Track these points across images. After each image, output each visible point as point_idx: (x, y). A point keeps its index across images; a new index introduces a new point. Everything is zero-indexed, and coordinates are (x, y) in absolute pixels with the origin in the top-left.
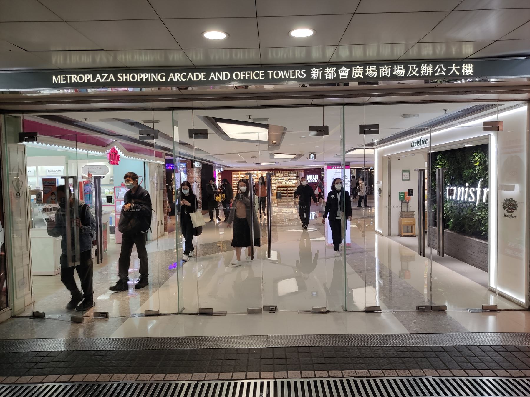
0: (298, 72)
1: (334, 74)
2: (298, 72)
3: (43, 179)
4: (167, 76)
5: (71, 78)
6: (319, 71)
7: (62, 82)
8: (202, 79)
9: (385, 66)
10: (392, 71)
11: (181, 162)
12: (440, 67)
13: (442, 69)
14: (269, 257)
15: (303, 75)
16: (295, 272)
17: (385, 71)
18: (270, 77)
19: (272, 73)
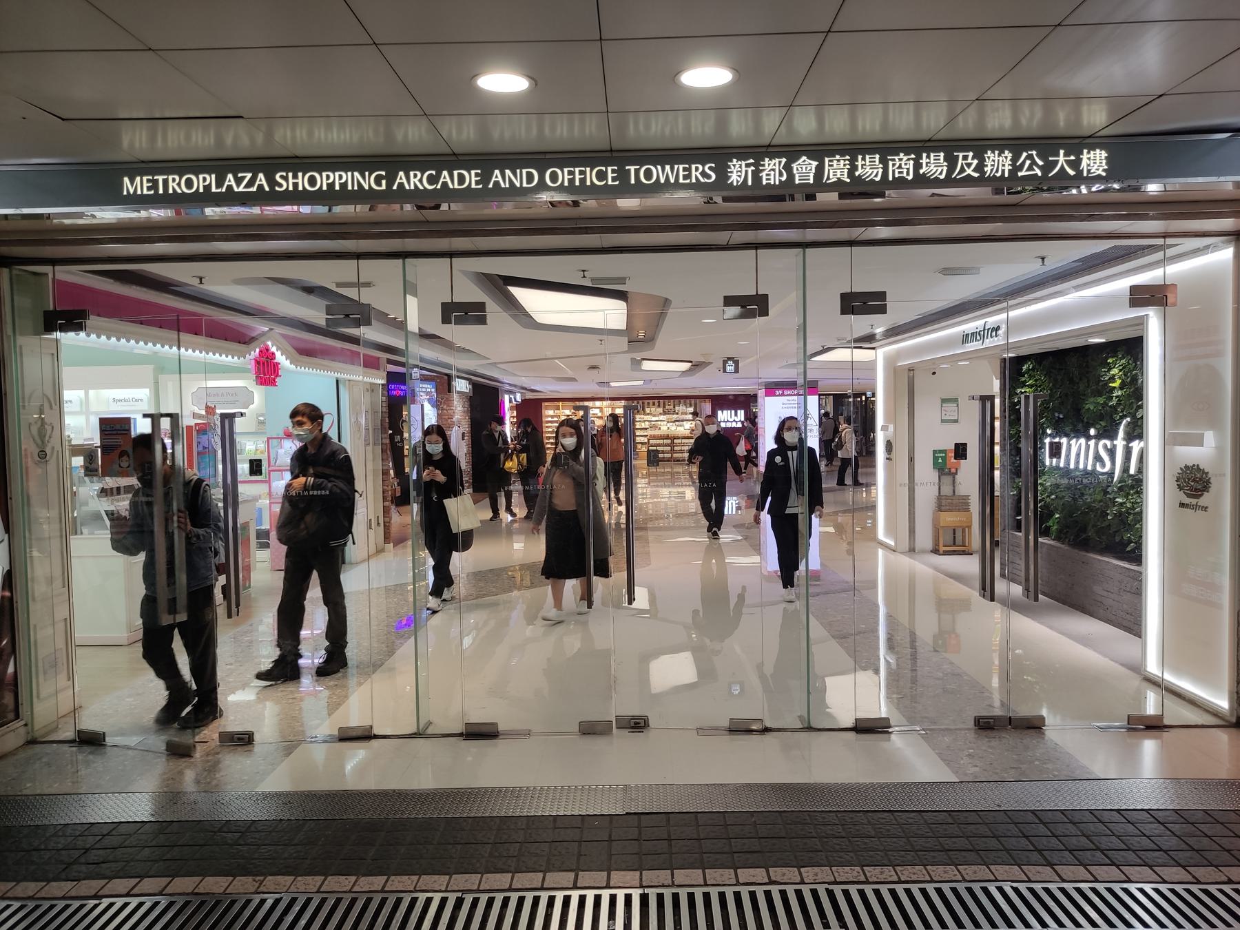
0: (697, 169)
1: (781, 174)
2: (697, 169)
4: (391, 179)
5: (166, 182)
6: (748, 166)
7: (145, 192)
8: (473, 186)
9: (902, 155)
10: (918, 166)
11: (425, 379)
12: (1030, 157)
13: (1034, 163)
15: (709, 177)
16: (690, 636)
17: (900, 167)
18: (633, 182)
19: (637, 172)
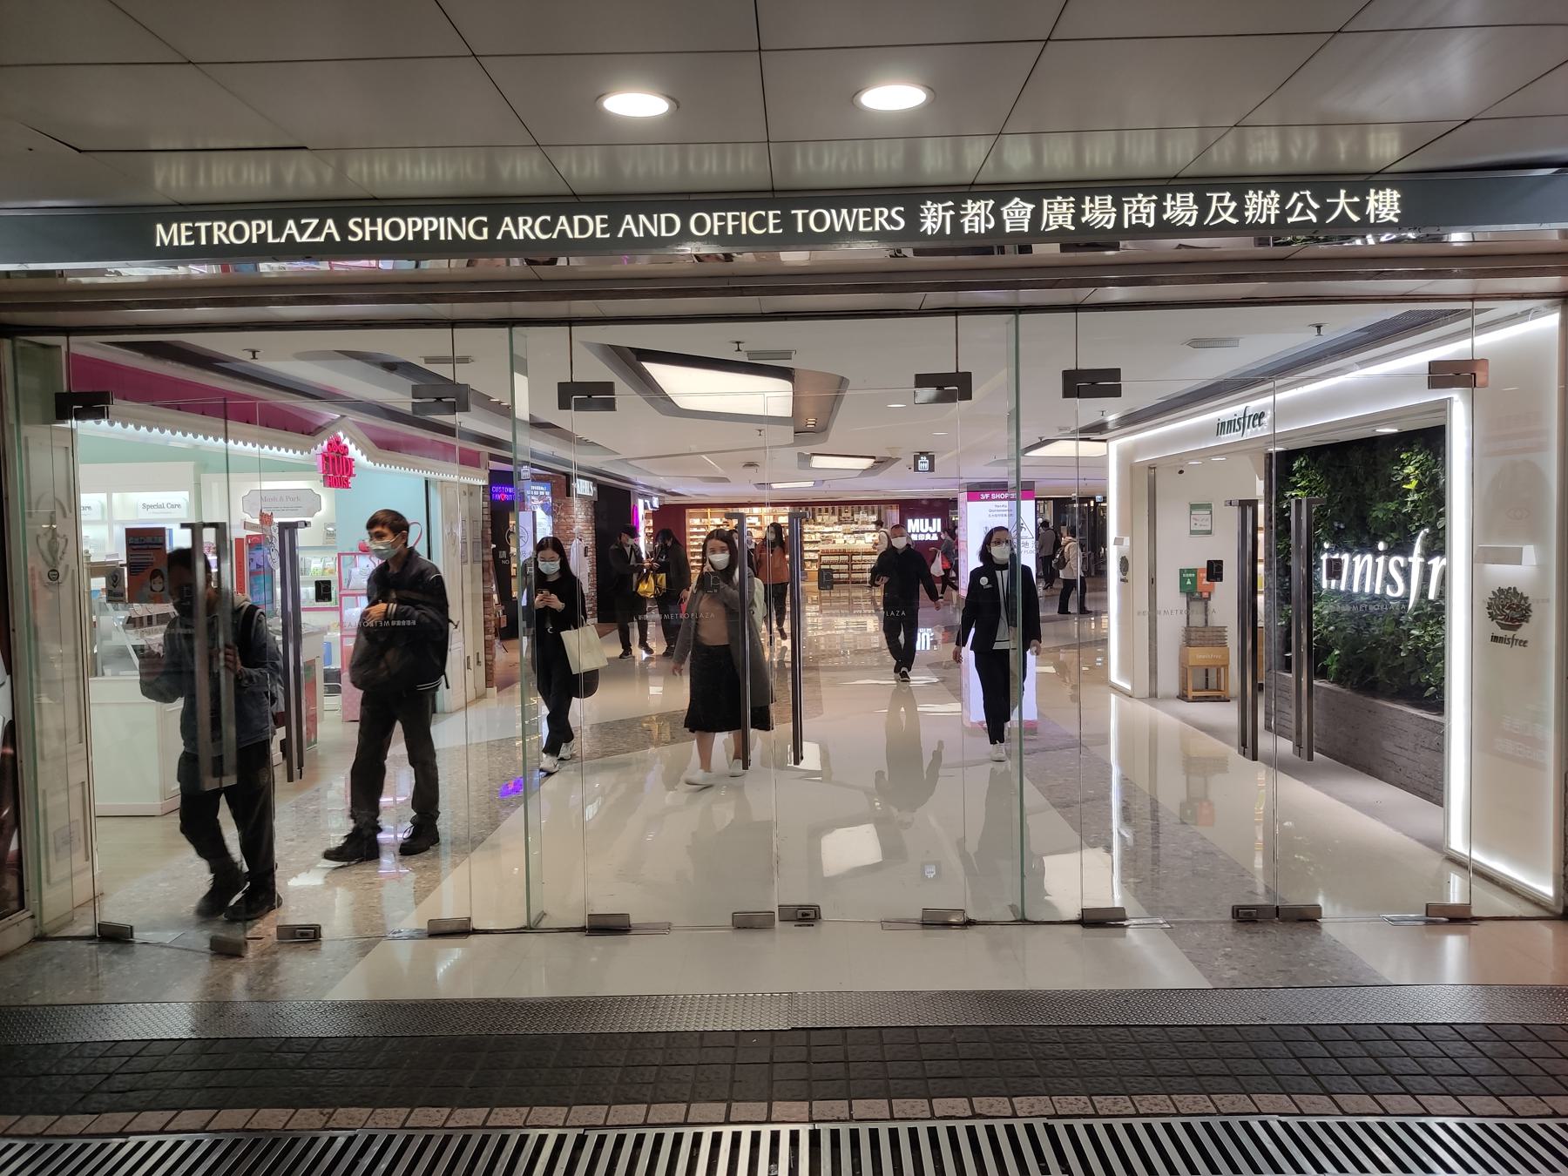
0: (881, 214)
1: (987, 221)
2: (881, 214)
4: (494, 226)
5: (209, 230)
6: (945, 209)
7: (184, 243)
8: (598, 235)
9: (1140, 196)
10: (1160, 210)
11: (537, 479)
12: (1302, 198)
13: (1307, 206)
14: (797, 762)
15: (896, 223)
17: (1138, 211)
18: (800, 230)
19: (806, 217)
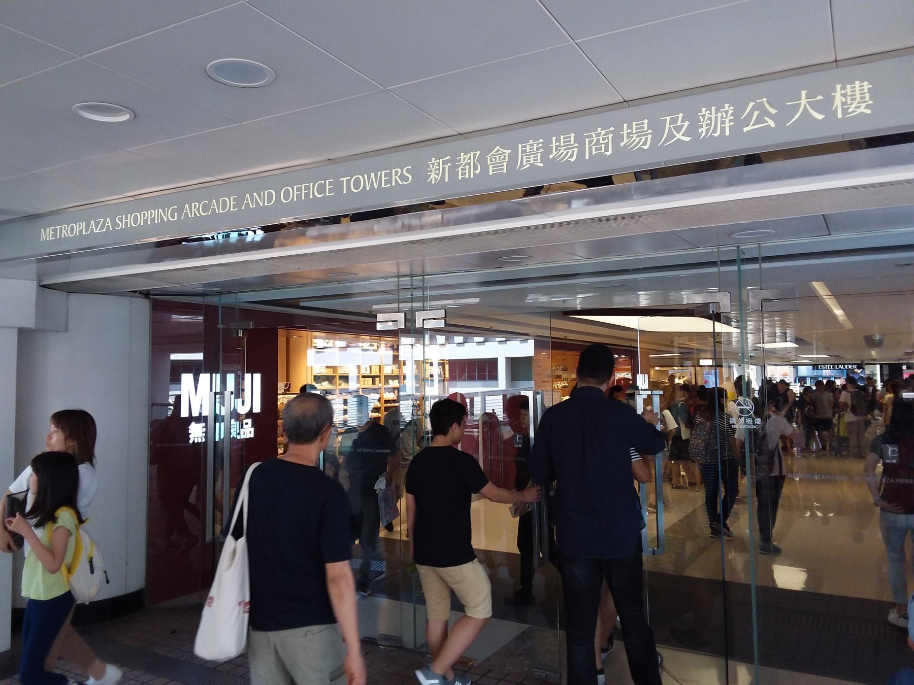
0: (397, 172)
1: (475, 168)
2: (397, 172)
3: (69, 592)
4: (180, 210)
6: (445, 163)
9: (531, 142)
10: (617, 138)
11: (388, 383)
12: (759, 107)
13: (764, 113)
15: (407, 179)
16: (792, 463)
17: (598, 142)
18: (587, 157)
19: (348, 182)
